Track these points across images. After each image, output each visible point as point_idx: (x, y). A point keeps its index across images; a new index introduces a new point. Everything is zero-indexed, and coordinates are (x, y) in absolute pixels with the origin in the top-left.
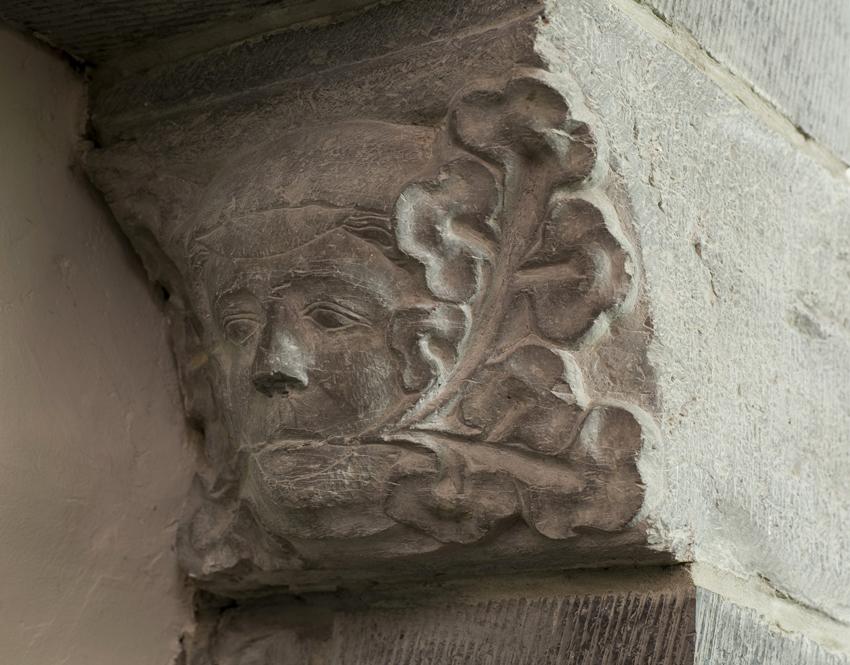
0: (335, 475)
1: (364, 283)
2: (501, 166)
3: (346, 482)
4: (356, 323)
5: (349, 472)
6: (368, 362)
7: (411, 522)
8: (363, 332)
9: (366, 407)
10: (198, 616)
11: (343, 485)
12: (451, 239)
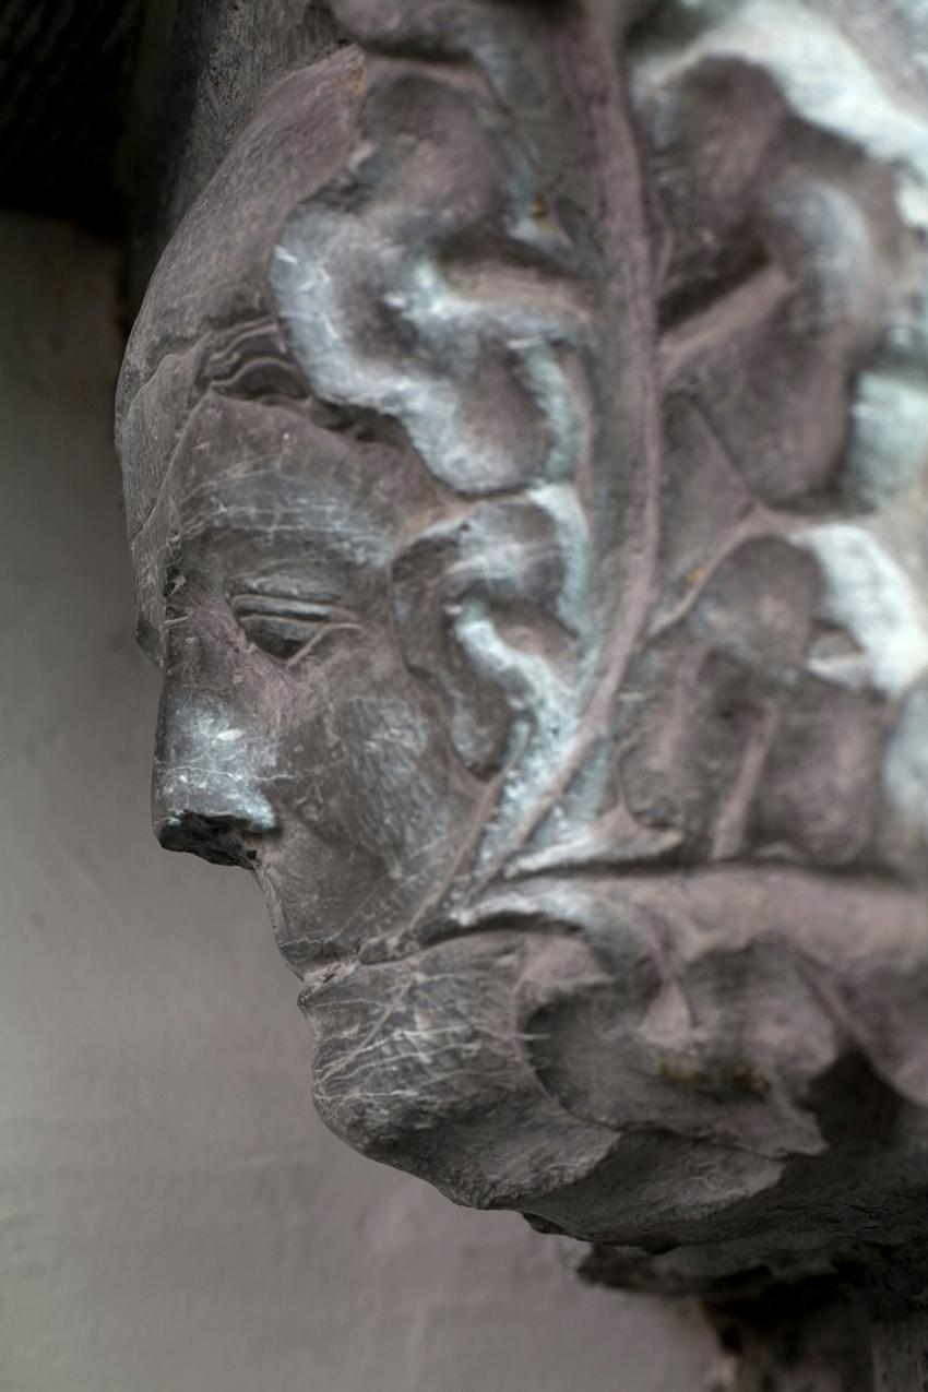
0: (392, 1044)
1: (287, 518)
2: (460, 59)
3: (424, 1057)
4: (328, 627)
5: (421, 1031)
6: (369, 723)
7: (648, 1123)
8: (351, 647)
9: (398, 846)
10: (731, 1342)
11: (420, 1067)
12: (445, 317)
